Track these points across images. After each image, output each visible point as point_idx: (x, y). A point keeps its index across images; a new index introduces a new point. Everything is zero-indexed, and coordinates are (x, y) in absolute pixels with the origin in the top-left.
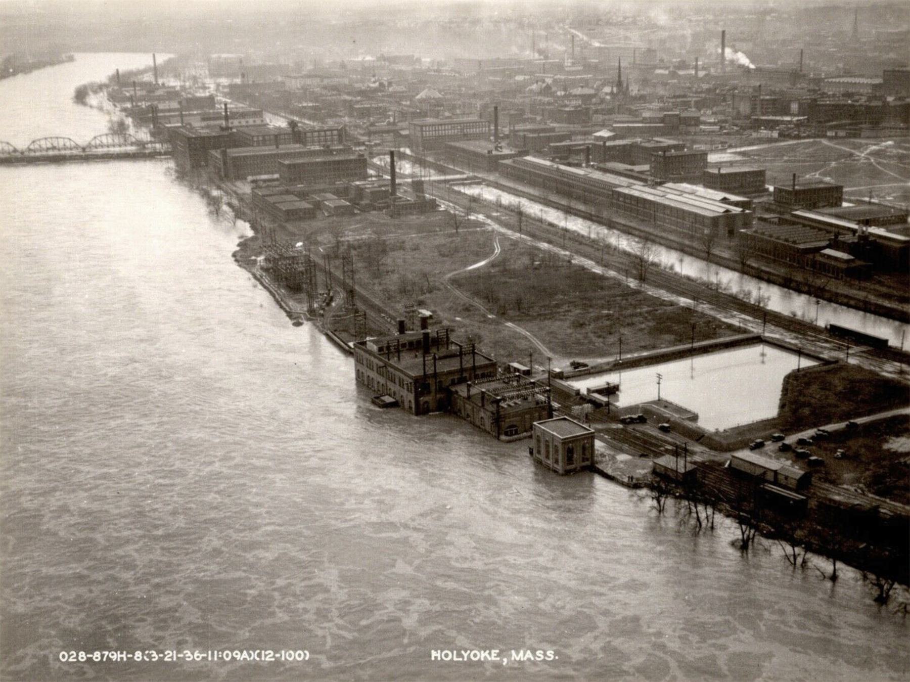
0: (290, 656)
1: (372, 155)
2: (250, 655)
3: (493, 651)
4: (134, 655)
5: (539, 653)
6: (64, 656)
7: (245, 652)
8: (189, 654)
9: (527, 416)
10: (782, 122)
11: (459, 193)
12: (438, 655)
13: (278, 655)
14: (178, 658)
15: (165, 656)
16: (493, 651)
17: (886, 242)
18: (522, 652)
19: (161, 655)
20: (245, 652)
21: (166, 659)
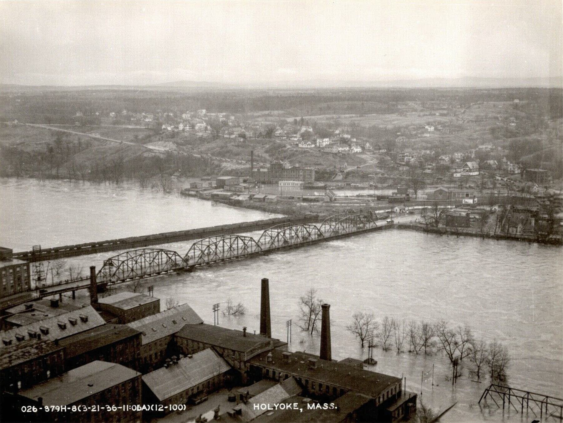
0: (175, 408)
1: (182, 112)
2: (147, 408)
3: (294, 404)
4: (71, 408)
5: (326, 405)
6: (24, 409)
7: (144, 406)
8: (109, 407)
9: (55, 355)
10: (336, 206)
11: (23, 260)
12: (258, 406)
13: (166, 407)
14: (123, 407)
15: (92, 408)
16: (294, 404)
17: (81, 337)
18: (314, 405)
19: (89, 408)
20: (144, 406)
21: (93, 410)
